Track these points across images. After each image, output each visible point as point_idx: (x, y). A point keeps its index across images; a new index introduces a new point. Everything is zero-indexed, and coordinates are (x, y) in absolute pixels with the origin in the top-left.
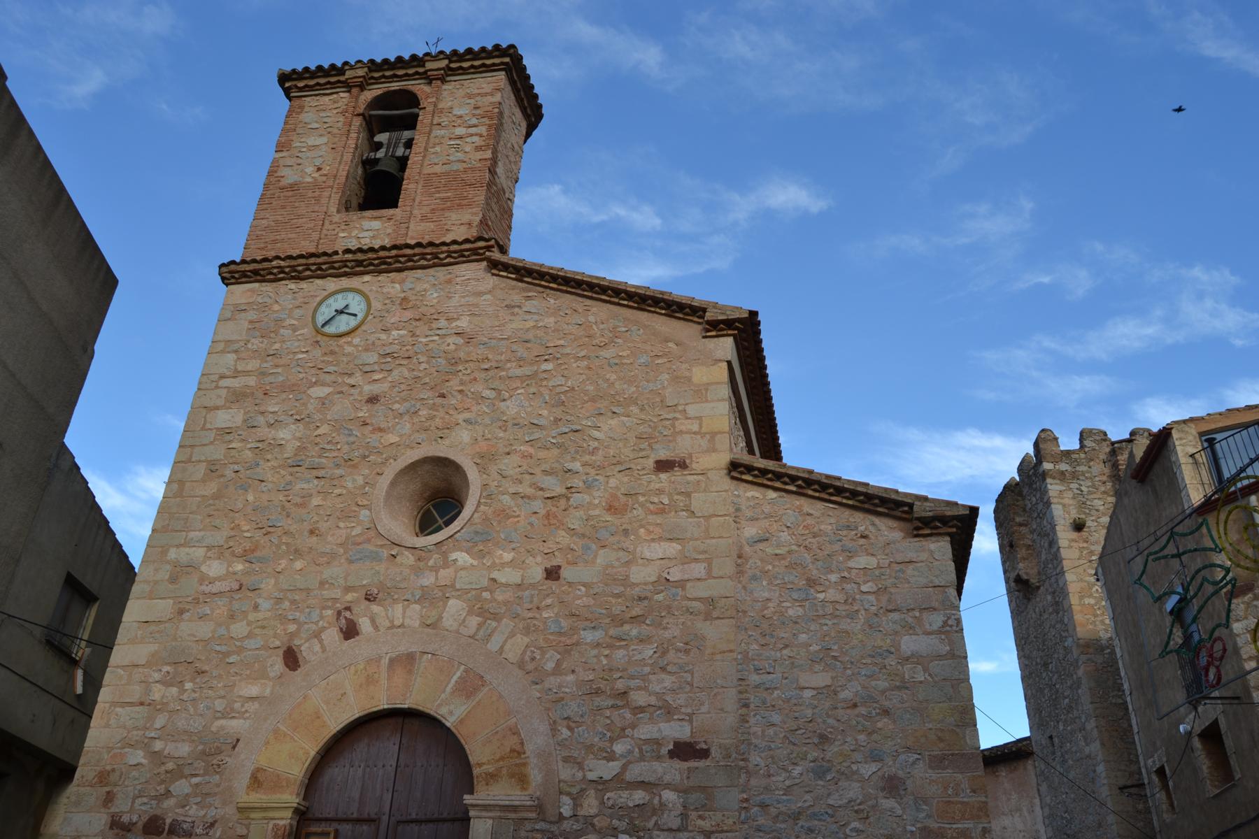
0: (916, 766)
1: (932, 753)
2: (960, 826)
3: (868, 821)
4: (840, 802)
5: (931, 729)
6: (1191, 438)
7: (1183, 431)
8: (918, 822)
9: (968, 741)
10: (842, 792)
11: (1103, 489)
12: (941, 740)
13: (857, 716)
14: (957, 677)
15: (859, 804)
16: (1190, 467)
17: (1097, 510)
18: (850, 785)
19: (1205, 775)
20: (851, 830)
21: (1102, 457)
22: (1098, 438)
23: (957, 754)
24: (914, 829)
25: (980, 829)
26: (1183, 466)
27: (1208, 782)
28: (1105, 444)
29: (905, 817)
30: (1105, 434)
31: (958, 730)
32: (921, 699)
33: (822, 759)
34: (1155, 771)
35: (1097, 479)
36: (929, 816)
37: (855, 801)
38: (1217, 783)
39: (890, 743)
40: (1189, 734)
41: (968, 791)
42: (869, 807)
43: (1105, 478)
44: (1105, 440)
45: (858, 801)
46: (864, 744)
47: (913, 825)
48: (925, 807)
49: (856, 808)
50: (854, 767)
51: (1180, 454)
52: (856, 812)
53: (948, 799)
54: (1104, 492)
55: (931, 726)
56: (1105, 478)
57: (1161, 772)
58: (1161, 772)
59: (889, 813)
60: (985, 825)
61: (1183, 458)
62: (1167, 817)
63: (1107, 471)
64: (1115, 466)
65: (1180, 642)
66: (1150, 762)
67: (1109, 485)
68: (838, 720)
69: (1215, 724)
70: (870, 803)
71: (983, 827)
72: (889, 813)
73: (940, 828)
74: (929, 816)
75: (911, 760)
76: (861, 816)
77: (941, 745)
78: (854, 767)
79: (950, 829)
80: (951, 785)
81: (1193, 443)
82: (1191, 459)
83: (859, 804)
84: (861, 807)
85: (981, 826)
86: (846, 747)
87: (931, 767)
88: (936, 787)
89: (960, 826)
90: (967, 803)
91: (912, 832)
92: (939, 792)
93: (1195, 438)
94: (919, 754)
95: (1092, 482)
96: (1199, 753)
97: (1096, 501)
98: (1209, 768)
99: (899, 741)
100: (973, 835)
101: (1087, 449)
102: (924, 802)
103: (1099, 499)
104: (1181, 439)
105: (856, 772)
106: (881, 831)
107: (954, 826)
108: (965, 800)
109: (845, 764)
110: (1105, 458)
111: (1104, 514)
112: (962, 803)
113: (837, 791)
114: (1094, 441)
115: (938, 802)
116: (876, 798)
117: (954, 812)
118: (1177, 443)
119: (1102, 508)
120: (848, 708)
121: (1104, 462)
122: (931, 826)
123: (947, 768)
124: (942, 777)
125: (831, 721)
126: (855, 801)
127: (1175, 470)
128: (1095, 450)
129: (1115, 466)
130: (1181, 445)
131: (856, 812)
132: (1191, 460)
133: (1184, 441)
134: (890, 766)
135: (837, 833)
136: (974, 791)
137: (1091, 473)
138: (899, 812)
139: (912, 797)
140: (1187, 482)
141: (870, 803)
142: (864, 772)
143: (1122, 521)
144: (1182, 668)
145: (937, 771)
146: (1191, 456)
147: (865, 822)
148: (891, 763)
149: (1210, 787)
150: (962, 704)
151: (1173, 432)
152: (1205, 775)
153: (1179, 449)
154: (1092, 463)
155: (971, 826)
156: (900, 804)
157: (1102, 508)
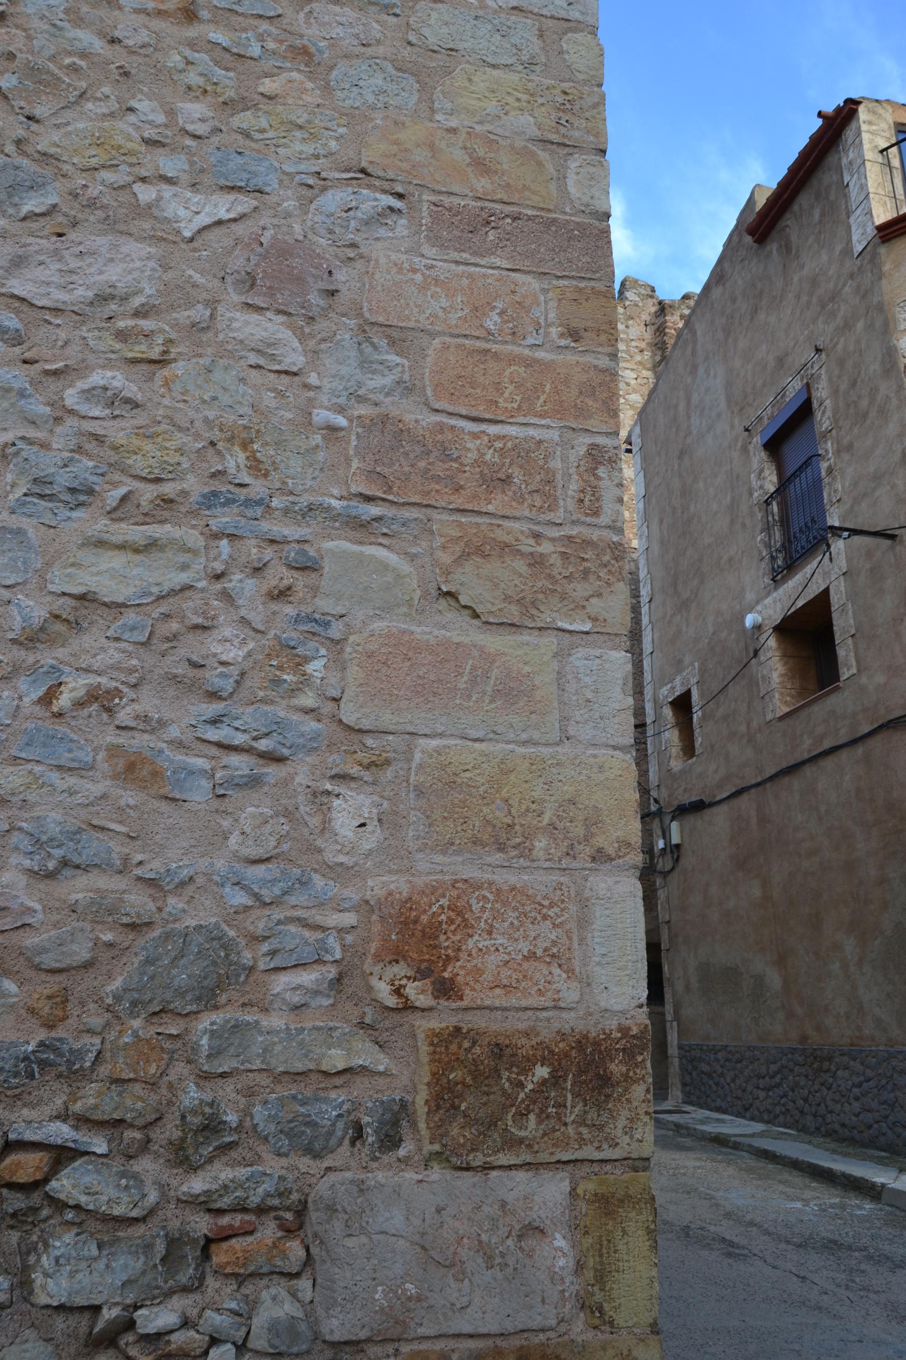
0: (382, 232)
1: (447, 200)
2: (512, 430)
3: (165, 372)
4: (59, 296)
5: (453, 131)
6: (884, 126)
7: (874, 113)
8: (361, 399)
9: (573, 190)
10: (74, 264)
11: (638, 358)
12: (481, 166)
13: (192, 44)
14: (562, 14)
15: (139, 313)
16: (877, 168)
17: (628, 384)
18: (115, 247)
19: (774, 686)
20: (88, 394)
21: (645, 317)
22: (643, 292)
23: (530, 218)
24: (341, 421)
25: (582, 450)
26: (868, 164)
27: (777, 695)
28: (650, 302)
29: (313, 379)
30: (653, 290)
31: (543, 155)
32: (432, 41)
33: (18, 142)
34: (671, 703)
35: (634, 344)
36: (406, 388)
37: (125, 299)
38: (788, 699)
39: (298, 147)
40: (758, 628)
41: (554, 331)
42: (175, 325)
43: (643, 345)
44: (652, 297)
45: (137, 301)
46: (201, 129)
47: (341, 410)
48: (393, 358)
49: (121, 324)
50: (145, 194)
51: (866, 146)
52: (122, 336)
53: (479, 344)
54: (640, 363)
55: (453, 123)
56: (643, 345)
57: (682, 705)
58: (682, 705)
59: (253, 359)
60: (600, 440)
61: (870, 154)
62: (676, 765)
63: (648, 335)
64: (660, 330)
65: (772, 489)
66: (665, 690)
67: (647, 354)
68: (113, 41)
69: (687, 695)
70: (184, 316)
71: (594, 446)
72: (253, 359)
73: (441, 428)
74: (406, 388)
75: (367, 208)
76: (140, 350)
77: (482, 184)
78: (145, 194)
79: (475, 436)
80: (500, 305)
81: (887, 134)
82: (880, 155)
83: (139, 313)
84: (147, 324)
85: (588, 440)
86: (125, 126)
87: (435, 240)
88: (444, 302)
89: (512, 430)
90: (546, 367)
91: (332, 429)
92: (453, 318)
93: (890, 128)
94: (400, 196)
95: (627, 346)
96: (769, 654)
97: (628, 372)
98: (782, 675)
99: (333, 144)
100: (556, 464)
101: (627, 303)
102: (392, 342)
103: (632, 370)
104: (870, 123)
105: (147, 211)
106: (211, 414)
107: (493, 429)
108: (541, 354)
109: (107, 176)
110: (648, 319)
111: (635, 391)
112: (529, 363)
113: (56, 254)
114: (639, 295)
115: (446, 347)
116: (212, 304)
117: (498, 387)
118: (864, 127)
119: (633, 382)
120: (160, 13)
121: (646, 325)
122: (407, 418)
123: (491, 252)
124: (470, 276)
125: (87, 38)
126: (125, 299)
127: (846, 178)
128: (637, 305)
129: (660, 330)
130: (868, 132)
131: (122, 336)
132: (880, 158)
133: (874, 128)
134: (288, 215)
135: (22, 394)
136: (574, 335)
137: (627, 334)
138: (295, 359)
139: (352, 323)
140: (871, 190)
141: (184, 316)
142: (182, 212)
143: (699, 333)
144: (768, 529)
145: (455, 255)
146: (882, 152)
147: (150, 378)
148: (290, 204)
149: (778, 704)
150: (566, 86)
151: (861, 109)
152: (774, 686)
153: (865, 136)
154: (631, 322)
155: (554, 435)
156: (302, 338)
157: (633, 382)
